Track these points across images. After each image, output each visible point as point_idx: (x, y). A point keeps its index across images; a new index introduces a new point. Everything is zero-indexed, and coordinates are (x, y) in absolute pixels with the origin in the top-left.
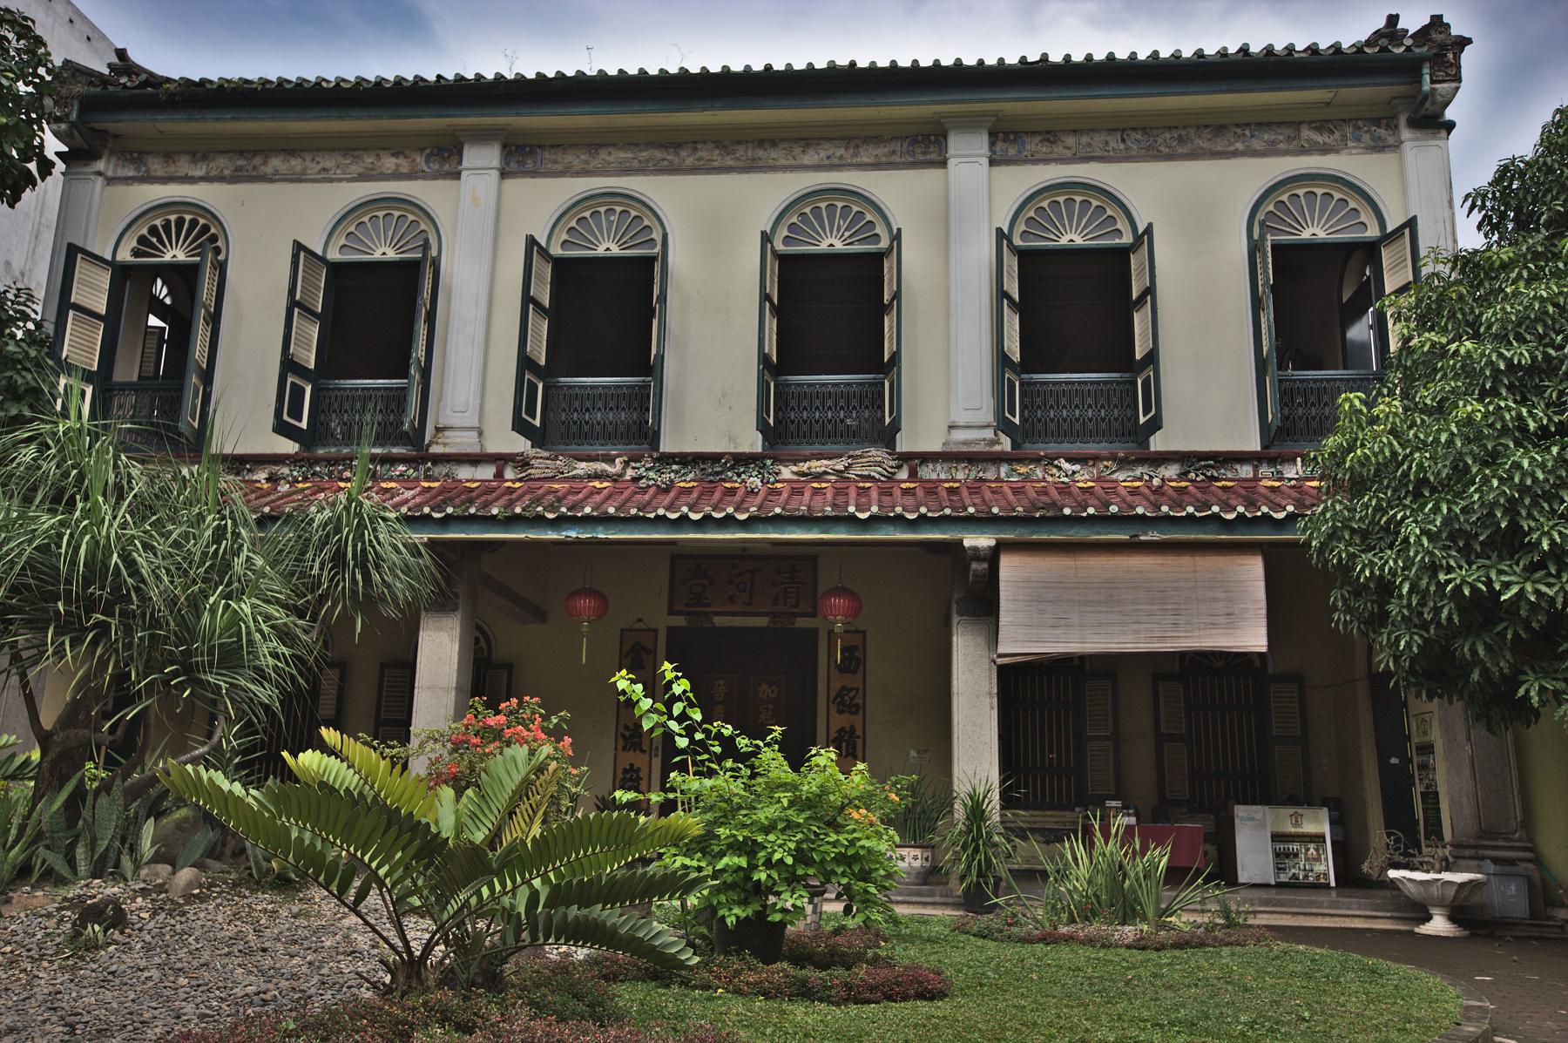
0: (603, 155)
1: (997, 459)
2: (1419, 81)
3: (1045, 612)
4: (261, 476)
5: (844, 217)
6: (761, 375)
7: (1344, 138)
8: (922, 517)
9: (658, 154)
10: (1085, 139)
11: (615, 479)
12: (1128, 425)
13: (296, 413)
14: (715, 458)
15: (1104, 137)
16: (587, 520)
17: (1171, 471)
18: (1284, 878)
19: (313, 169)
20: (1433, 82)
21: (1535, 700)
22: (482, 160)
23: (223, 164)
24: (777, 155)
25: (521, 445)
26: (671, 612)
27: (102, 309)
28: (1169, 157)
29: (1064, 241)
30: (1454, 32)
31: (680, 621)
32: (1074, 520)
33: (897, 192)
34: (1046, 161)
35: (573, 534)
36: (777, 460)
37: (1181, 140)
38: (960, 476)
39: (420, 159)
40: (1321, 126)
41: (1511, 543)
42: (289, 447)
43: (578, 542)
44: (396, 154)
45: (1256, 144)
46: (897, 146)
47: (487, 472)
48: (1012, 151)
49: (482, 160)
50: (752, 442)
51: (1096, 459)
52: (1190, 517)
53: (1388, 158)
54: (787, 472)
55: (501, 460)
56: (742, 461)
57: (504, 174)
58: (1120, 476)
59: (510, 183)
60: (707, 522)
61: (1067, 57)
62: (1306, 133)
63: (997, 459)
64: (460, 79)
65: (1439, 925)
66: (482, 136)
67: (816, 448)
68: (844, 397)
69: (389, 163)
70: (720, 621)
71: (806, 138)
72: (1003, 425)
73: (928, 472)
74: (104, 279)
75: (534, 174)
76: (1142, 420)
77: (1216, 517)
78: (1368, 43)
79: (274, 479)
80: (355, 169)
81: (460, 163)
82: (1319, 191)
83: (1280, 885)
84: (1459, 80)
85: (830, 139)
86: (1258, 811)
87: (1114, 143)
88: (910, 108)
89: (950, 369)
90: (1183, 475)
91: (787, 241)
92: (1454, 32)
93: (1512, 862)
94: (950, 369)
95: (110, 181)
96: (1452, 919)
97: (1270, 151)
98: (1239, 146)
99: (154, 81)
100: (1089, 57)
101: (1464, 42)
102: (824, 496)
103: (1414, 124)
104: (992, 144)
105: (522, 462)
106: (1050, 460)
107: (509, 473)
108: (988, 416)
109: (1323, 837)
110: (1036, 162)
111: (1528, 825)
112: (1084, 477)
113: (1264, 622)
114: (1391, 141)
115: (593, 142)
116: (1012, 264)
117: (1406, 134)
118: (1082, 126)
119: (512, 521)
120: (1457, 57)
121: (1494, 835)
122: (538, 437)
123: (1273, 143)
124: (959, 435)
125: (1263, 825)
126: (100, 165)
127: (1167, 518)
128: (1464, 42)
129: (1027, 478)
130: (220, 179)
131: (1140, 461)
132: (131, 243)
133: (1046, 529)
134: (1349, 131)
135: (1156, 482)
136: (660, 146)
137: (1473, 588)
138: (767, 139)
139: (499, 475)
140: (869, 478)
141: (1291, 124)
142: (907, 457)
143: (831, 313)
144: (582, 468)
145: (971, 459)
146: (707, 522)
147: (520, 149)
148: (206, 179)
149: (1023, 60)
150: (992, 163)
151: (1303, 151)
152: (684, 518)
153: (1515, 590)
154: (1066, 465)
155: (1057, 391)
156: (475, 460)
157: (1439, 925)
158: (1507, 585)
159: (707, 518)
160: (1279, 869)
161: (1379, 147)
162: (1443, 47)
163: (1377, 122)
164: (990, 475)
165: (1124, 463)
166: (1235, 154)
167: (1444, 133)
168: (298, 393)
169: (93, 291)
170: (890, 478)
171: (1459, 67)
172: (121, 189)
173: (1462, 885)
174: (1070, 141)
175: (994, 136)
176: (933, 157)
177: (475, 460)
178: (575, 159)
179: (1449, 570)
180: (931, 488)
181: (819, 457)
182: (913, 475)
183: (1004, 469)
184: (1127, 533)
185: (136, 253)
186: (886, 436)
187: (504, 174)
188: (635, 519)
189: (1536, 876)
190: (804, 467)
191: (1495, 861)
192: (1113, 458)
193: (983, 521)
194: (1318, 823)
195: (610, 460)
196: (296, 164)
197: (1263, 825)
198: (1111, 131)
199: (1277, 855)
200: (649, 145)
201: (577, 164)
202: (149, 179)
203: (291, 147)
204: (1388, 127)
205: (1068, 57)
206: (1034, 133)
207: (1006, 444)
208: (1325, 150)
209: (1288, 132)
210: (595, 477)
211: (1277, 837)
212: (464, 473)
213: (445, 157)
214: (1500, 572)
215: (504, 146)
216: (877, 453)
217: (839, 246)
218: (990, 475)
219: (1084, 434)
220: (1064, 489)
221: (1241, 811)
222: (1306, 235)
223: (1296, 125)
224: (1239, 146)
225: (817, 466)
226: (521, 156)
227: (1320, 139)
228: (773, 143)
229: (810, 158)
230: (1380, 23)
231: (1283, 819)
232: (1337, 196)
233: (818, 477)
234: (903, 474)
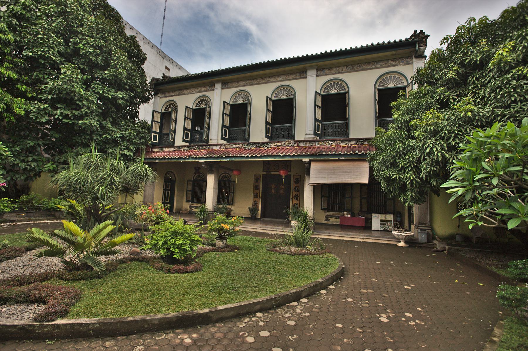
0: (240, 83)
1: (315, 141)
2: (416, 47)
3: (319, 175)
4: (182, 149)
5: (281, 92)
6: (266, 126)
7: (399, 62)
8: (294, 155)
9: (250, 81)
10: (338, 69)
11: (240, 148)
12: (343, 132)
13: (187, 137)
14: (259, 143)
15: (342, 68)
16: (231, 157)
17: (353, 143)
18: (382, 229)
19: (191, 91)
20: (419, 47)
21: (402, 201)
22: (218, 86)
23: (177, 93)
24: (273, 79)
25: (224, 142)
26: (263, 171)
27: (159, 121)
28: (357, 71)
29: (333, 92)
30: (426, 34)
31: (265, 173)
32: (326, 155)
33: (297, 85)
34: (329, 75)
35: (228, 160)
36: (270, 143)
37: (360, 67)
38: (307, 145)
39: (208, 88)
40: (393, 60)
41: (394, 165)
42: (186, 144)
43: (229, 161)
44: (204, 87)
45: (378, 66)
46: (297, 75)
47: (218, 147)
48: (322, 73)
49: (218, 86)
50: (267, 140)
51: (337, 140)
52: (351, 154)
53: (410, 66)
54: (273, 145)
55: (221, 145)
56: (264, 143)
57: (222, 89)
58: (342, 144)
59: (223, 90)
60: (252, 157)
61: (331, 51)
62: (390, 62)
63: (315, 141)
64: (273, 61)
65: (402, 244)
66: (218, 82)
67: (278, 140)
68: (285, 129)
69: (203, 89)
70: (272, 173)
71: (278, 75)
72: (315, 134)
73: (301, 144)
74: (159, 115)
75: (227, 88)
76: (320, 133)
77: (357, 154)
78: (410, 38)
79: (184, 150)
80: (197, 91)
81: (306, 74)
82: (388, 76)
83: (381, 231)
84: (426, 45)
85: (283, 75)
86: (377, 215)
87: (344, 69)
88: (298, 66)
89: (305, 125)
90: (356, 144)
91: (324, 91)
92: (426, 34)
93: (425, 230)
94: (305, 125)
95: (161, 98)
96: (405, 242)
97: (381, 67)
98: (374, 67)
99: (170, 78)
100: (336, 50)
101: (428, 36)
102: (281, 150)
103: (416, 57)
104: (317, 72)
105: (224, 145)
106: (327, 141)
107: (222, 148)
108: (312, 132)
109: (391, 221)
110: (327, 75)
111: (431, 221)
112: (334, 144)
113: (368, 177)
114: (411, 62)
115: (238, 81)
116: (319, 98)
117: (414, 60)
118: (337, 66)
119: (218, 158)
120: (426, 40)
121: (422, 224)
122: (228, 140)
123: (382, 65)
124: (308, 136)
125: (378, 218)
126: (159, 95)
127: (346, 154)
128: (428, 36)
129: (321, 145)
130: (177, 95)
131: (346, 140)
132: (164, 108)
133: (321, 157)
134: (400, 60)
135: (349, 145)
136: (251, 80)
137: (386, 176)
138: (271, 76)
139: (220, 148)
140: (288, 146)
141: (386, 60)
142: (297, 141)
143: (283, 112)
144: (235, 146)
145: (310, 141)
146: (252, 157)
147: (225, 83)
148: (175, 95)
149: (321, 53)
150: (317, 76)
151: (389, 66)
152: (248, 156)
153: (395, 176)
154: (330, 142)
155: (330, 126)
156: (216, 145)
157: (402, 244)
158: (393, 175)
159: (252, 156)
160: (381, 227)
161: (408, 64)
162: (422, 38)
163: (407, 58)
164: (314, 145)
165: (343, 141)
166: (373, 69)
167: (424, 59)
168: (269, 128)
169: (158, 118)
170: (293, 146)
171: (426, 42)
172: (162, 99)
173: (406, 236)
174: (335, 69)
175: (317, 70)
176: (305, 76)
177: (216, 145)
178: (235, 84)
179: (383, 171)
180: (301, 148)
181: (279, 142)
182: (298, 145)
183: (317, 143)
184: (337, 157)
185: (165, 110)
186: (292, 137)
187: (222, 89)
188: (239, 157)
189: (431, 233)
190: (276, 144)
191: (421, 230)
192: (340, 140)
193: (306, 156)
194: (391, 217)
195: (239, 144)
196: (188, 91)
197: (378, 218)
198: (344, 66)
199: (381, 224)
200: (249, 80)
201: (235, 85)
202: (166, 97)
203: (187, 88)
204: (410, 58)
205: (351, 48)
206: (326, 68)
207: (318, 138)
208: (394, 66)
209: (385, 62)
210: (237, 147)
211: (381, 220)
212: (215, 147)
213: (211, 86)
214: (392, 172)
215: (222, 83)
216: (290, 141)
217: (285, 97)
218: (314, 145)
219: (335, 135)
220: (328, 147)
221: (373, 215)
222: (389, 86)
223: (387, 60)
224: (374, 67)
225: (278, 144)
226: (225, 85)
227: (393, 63)
228: (272, 77)
229: (279, 79)
230: (413, 33)
231: (383, 217)
232: (393, 76)
233: (279, 146)
234: (296, 145)
